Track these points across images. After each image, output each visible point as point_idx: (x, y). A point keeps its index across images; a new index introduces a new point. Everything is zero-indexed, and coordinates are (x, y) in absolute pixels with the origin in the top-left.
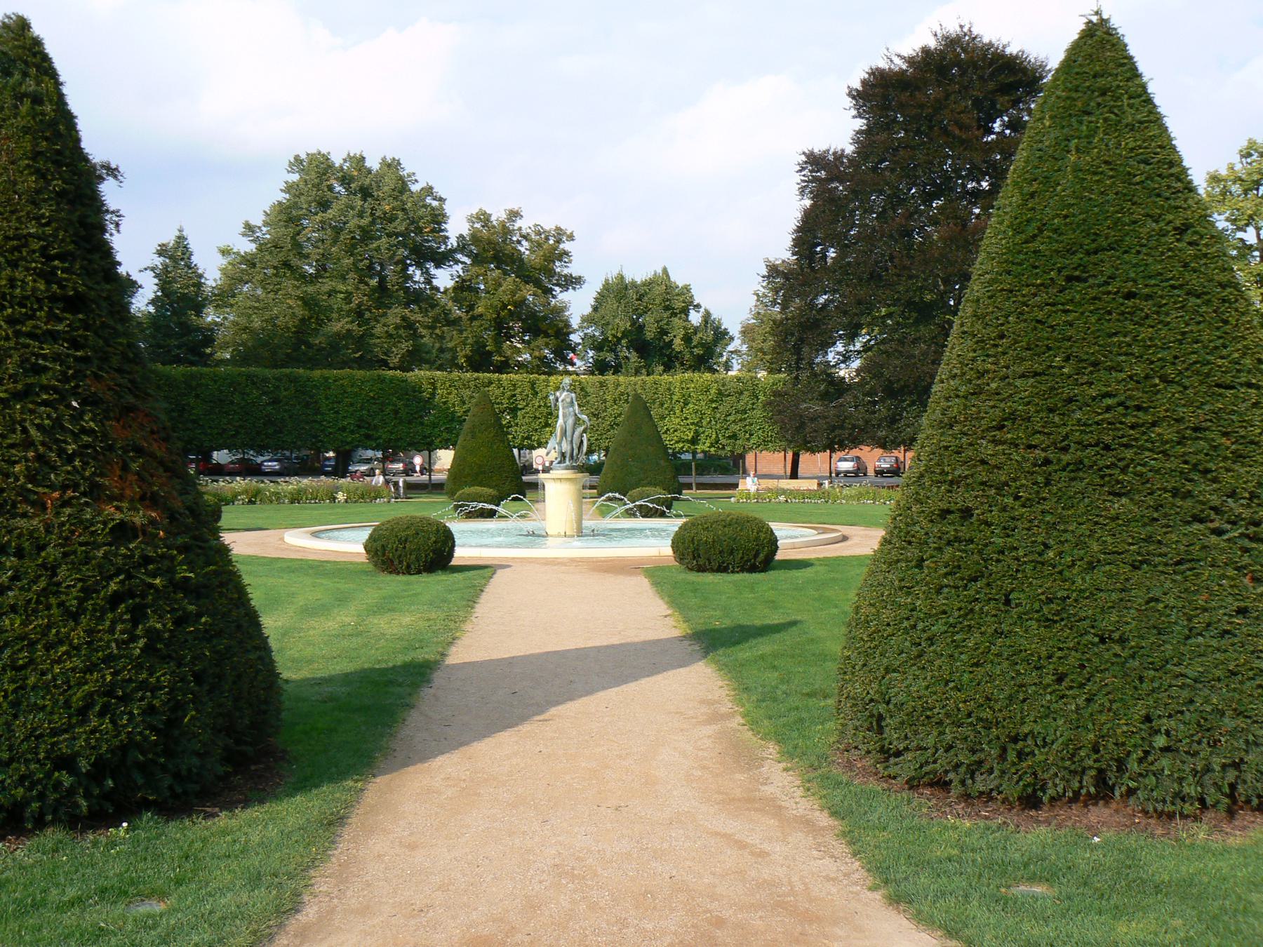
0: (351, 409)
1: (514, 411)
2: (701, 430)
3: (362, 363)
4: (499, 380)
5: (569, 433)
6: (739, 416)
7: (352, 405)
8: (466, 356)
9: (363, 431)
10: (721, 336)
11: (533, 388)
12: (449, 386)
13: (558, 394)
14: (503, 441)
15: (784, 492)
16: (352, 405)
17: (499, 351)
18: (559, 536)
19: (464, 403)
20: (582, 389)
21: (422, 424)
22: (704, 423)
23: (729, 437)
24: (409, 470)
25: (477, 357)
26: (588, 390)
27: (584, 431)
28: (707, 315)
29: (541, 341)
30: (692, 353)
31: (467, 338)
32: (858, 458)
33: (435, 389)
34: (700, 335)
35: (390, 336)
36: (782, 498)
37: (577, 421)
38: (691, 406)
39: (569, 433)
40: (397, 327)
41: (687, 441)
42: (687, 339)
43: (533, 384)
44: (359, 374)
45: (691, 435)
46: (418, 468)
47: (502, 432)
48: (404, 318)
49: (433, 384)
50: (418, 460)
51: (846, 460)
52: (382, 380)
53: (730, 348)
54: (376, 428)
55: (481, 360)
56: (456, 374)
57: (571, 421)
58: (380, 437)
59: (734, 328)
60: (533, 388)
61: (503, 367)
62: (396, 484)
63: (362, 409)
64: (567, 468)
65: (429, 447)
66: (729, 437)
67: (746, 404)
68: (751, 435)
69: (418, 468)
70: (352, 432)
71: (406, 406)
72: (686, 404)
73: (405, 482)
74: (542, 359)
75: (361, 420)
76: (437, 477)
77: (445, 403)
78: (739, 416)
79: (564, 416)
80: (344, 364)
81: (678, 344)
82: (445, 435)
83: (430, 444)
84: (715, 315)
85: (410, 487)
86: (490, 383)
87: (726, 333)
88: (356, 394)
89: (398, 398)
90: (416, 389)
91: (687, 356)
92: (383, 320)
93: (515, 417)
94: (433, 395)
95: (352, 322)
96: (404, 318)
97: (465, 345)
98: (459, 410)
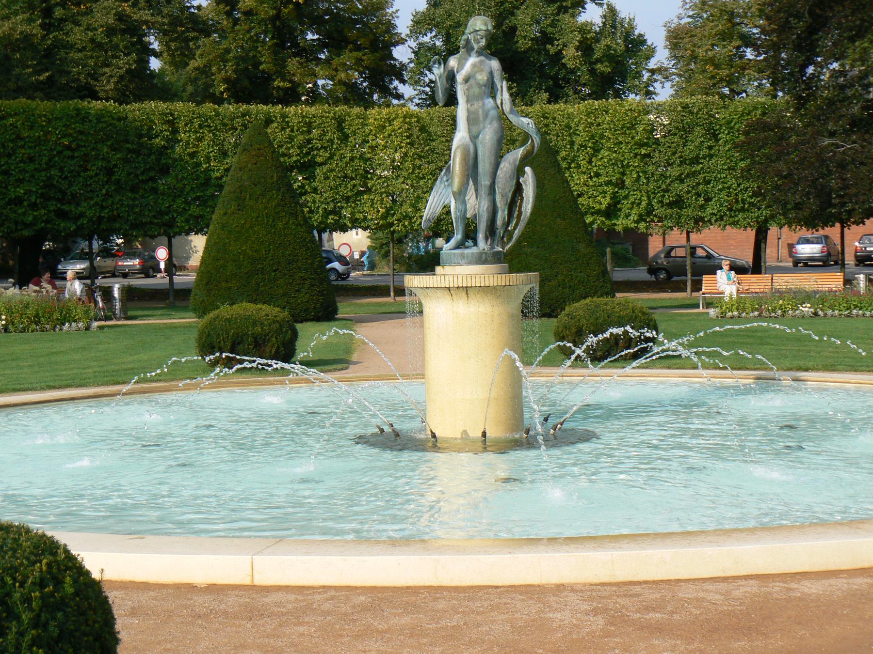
0: (31, 167)
1: (308, 167)
2: (623, 193)
3: (50, 90)
4: (284, 116)
5: (485, 166)
6: (687, 169)
7: (31, 160)
8: (226, 80)
9: (53, 206)
10: (636, 46)
11: (340, 127)
12: (204, 132)
13: (453, 62)
14: (295, 215)
15: (807, 296)
16: (31, 160)
17: (281, 73)
18: (464, 444)
19: (225, 154)
20: (423, 129)
21: (154, 190)
22: (628, 182)
23: (671, 205)
24: (149, 268)
25: (246, 83)
26: (432, 129)
27: (525, 160)
28: (612, 11)
29: (348, 57)
30: (592, 72)
31: (228, 51)
32: (826, 237)
33: (175, 131)
34: (605, 41)
35: (100, 46)
36: (806, 309)
37: (508, 138)
38: (604, 153)
39: (485, 166)
40: (110, 31)
41: (598, 212)
42: (586, 48)
43: (340, 122)
44: (42, 106)
45: (606, 202)
46: (162, 266)
47: (292, 197)
48: (121, 17)
49: (171, 123)
50: (162, 254)
51: (808, 241)
52: (82, 116)
53: (652, 64)
54: (75, 200)
55: (251, 86)
56: (208, 107)
57: (488, 135)
58: (82, 215)
59: (656, 36)
60: (340, 127)
61: (290, 97)
62: (107, 293)
63: (49, 166)
64: (481, 259)
65: (171, 229)
66: (671, 205)
67: (700, 147)
68: (708, 200)
69: (162, 266)
70: (34, 206)
71: (126, 160)
72: (596, 150)
73: (123, 290)
74: (352, 87)
75: (49, 185)
76: (184, 279)
77: (193, 155)
78: (687, 169)
79: (472, 120)
80: (19, 91)
81: (571, 55)
82: (195, 210)
83: (170, 225)
84: (624, 13)
85: (131, 295)
86: (268, 121)
87: (641, 41)
88: (38, 142)
89: (113, 148)
90: (144, 132)
91: (585, 78)
92: (85, 20)
93: (311, 178)
94: (173, 141)
95: (30, 21)
96: (121, 17)
97: (225, 61)
98: (217, 169)
